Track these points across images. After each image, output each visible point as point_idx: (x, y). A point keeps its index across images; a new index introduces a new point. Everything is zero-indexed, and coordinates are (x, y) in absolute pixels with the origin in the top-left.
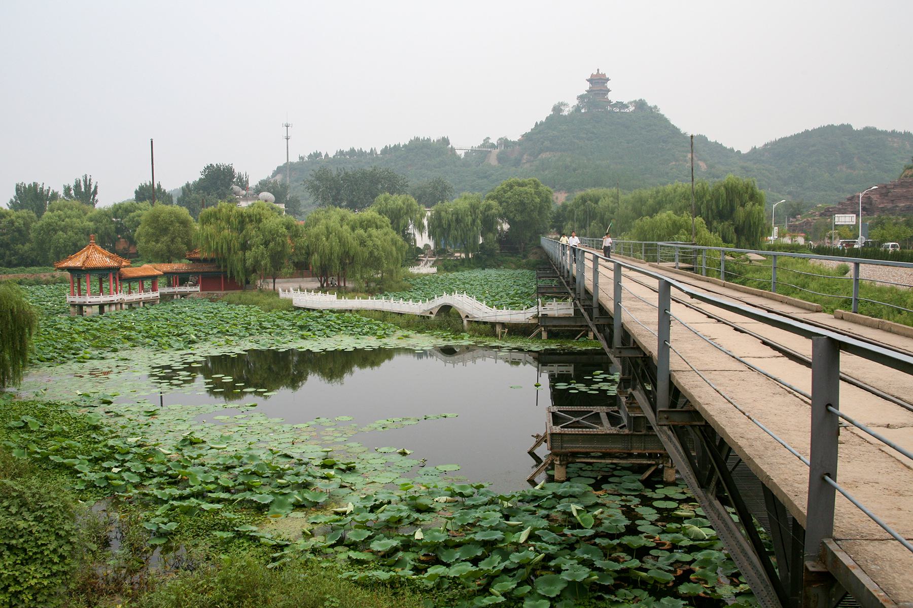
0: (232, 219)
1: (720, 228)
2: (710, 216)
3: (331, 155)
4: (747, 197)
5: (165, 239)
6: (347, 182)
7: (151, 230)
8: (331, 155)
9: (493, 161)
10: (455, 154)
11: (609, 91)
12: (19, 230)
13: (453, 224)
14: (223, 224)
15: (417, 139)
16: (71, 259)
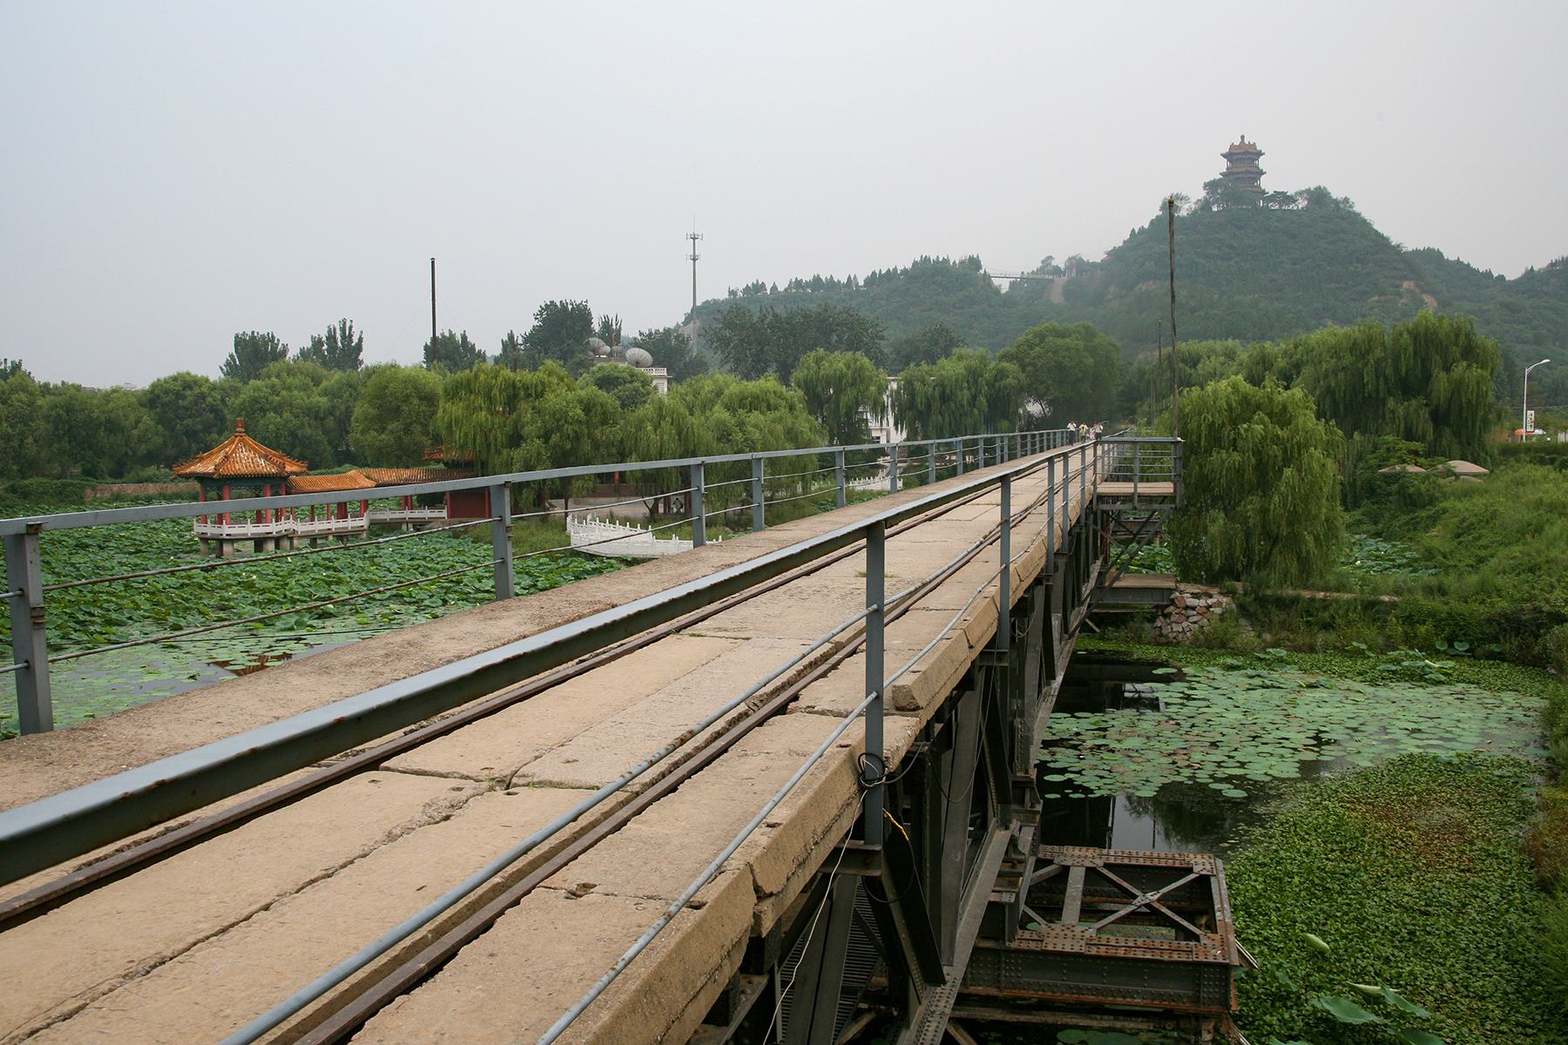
0: (495, 392)
1: (1401, 411)
2: (1382, 387)
3: (781, 289)
4: (1455, 351)
5: (393, 426)
6: (764, 333)
7: (371, 411)
8: (781, 289)
9: (1057, 297)
10: (990, 284)
11: (1262, 173)
12: (214, 410)
13: (936, 404)
14: (480, 401)
15: (926, 260)
16: (202, 459)
